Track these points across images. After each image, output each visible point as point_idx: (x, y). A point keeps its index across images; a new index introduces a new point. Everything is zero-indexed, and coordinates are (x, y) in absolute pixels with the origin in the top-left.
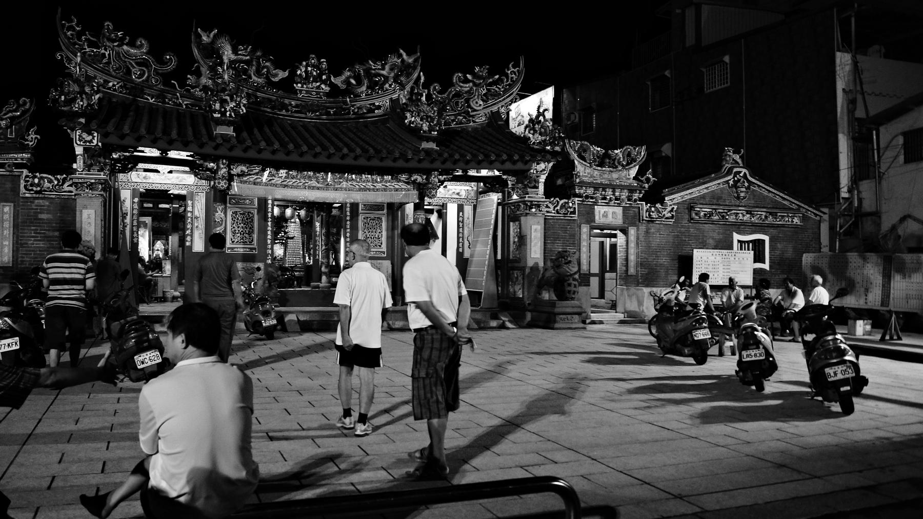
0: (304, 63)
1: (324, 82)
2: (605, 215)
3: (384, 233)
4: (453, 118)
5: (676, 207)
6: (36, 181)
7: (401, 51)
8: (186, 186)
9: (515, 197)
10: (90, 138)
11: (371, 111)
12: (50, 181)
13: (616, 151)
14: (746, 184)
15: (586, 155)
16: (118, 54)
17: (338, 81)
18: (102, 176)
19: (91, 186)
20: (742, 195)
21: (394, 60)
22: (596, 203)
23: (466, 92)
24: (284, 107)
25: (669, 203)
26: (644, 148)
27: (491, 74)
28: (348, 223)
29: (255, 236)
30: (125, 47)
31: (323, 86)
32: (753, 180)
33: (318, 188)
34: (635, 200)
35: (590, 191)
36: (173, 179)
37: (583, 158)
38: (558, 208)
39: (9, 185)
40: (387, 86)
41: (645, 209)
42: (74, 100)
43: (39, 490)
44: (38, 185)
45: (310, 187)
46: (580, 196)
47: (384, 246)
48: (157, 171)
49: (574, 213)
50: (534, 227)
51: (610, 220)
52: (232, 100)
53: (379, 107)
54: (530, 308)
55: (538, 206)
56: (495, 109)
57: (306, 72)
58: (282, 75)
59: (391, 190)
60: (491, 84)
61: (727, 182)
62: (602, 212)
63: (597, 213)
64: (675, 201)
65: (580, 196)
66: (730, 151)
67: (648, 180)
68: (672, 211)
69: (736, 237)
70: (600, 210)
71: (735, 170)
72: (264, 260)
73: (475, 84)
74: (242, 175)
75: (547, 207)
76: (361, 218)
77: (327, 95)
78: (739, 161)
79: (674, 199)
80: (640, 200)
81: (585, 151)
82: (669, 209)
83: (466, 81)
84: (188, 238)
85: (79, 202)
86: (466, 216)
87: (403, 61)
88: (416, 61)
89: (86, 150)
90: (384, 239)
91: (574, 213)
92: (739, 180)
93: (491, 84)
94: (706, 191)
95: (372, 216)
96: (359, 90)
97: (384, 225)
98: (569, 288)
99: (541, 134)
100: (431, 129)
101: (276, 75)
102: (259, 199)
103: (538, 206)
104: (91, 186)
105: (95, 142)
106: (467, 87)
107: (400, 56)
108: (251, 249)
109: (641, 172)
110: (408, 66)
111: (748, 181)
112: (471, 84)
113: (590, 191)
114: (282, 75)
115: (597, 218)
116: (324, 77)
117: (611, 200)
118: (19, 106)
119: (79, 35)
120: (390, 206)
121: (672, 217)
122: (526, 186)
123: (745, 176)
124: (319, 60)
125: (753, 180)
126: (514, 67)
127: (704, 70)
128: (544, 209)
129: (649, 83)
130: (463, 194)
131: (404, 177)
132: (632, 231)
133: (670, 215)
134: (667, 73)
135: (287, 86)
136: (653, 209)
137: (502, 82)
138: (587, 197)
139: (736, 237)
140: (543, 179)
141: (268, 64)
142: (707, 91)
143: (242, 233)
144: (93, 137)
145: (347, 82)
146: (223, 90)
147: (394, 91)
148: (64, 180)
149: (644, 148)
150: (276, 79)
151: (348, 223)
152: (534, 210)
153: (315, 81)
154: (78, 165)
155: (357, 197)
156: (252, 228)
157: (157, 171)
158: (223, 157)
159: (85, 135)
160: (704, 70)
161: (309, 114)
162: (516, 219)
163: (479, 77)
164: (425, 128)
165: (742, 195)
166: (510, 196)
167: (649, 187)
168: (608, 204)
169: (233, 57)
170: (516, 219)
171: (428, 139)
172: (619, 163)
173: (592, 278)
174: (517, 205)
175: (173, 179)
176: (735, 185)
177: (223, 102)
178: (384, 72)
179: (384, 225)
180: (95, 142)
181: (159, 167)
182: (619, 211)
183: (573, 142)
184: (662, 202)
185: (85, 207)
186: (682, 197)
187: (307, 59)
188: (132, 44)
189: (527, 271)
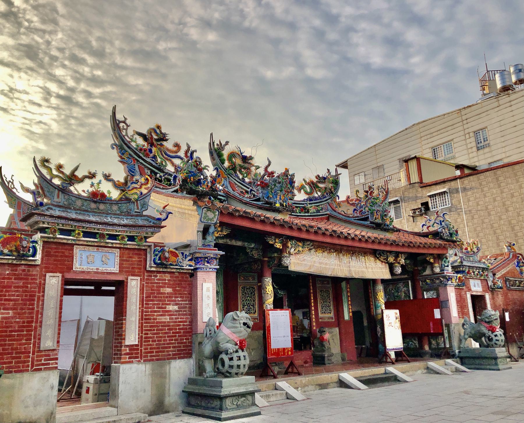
28: (312, 295)
144: (215, 215)
151: (312, 295)
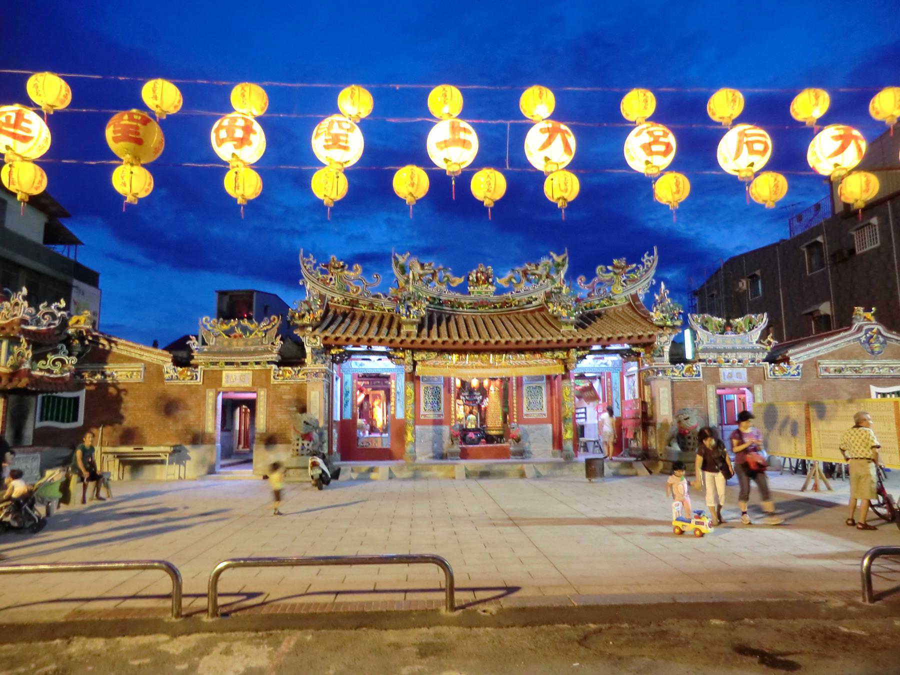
0: (475, 271)
1: (491, 284)
2: (730, 376)
3: (545, 399)
4: (597, 302)
5: (801, 365)
6: (281, 373)
7: (552, 253)
8: (390, 369)
9: (646, 365)
10: (315, 341)
11: (529, 302)
12: (290, 372)
13: (737, 320)
14: (881, 339)
15: (709, 326)
16: (341, 277)
17: (502, 282)
18: (324, 367)
19: (316, 375)
20: (877, 350)
21: (544, 260)
22: (720, 366)
23: (608, 281)
24: (461, 305)
25: (794, 362)
26: (765, 314)
27: (629, 262)
29: (442, 405)
30: (346, 272)
31: (490, 287)
32: (889, 335)
33: (483, 367)
34: (758, 362)
35: (712, 356)
36: (378, 364)
37: (706, 329)
38: (684, 372)
39: (264, 376)
40: (541, 282)
41: (769, 368)
42: (303, 316)
43: (174, 480)
44: (282, 375)
45: (476, 367)
46: (703, 361)
47: (545, 411)
48: (369, 360)
49: (699, 375)
50: (661, 389)
51: (736, 380)
52: (415, 305)
53: (536, 299)
54: (664, 458)
55: (664, 371)
56: (633, 292)
57: (477, 278)
58: (459, 281)
59: (541, 365)
60: (630, 272)
61: (859, 339)
62: (726, 374)
63: (721, 374)
64: (800, 360)
65: (703, 361)
66: (859, 310)
67: (770, 343)
68: (798, 368)
69: (874, 389)
70: (725, 371)
71: (866, 327)
72: (449, 423)
73: (615, 274)
74: (423, 360)
75: (673, 371)
76: (525, 387)
77: (496, 293)
78: (872, 318)
79: (799, 356)
80: (764, 361)
81: (707, 322)
82: (795, 367)
83: (608, 271)
84: (393, 408)
85: (309, 386)
86: (614, 381)
87: (553, 261)
88: (564, 260)
89: (313, 349)
90: (544, 404)
91: (699, 375)
92: (872, 337)
93: (630, 272)
94: (834, 349)
95: (534, 385)
96: (519, 287)
97: (544, 392)
98: (689, 441)
99: (662, 312)
100: (569, 315)
101: (453, 282)
102: (444, 378)
103: (664, 371)
104: (316, 375)
105: (318, 343)
106: (608, 276)
107: (551, 257)
108: (439, 415)
109: (764, 336)
110: (559, 265)
111: (883, 336)
112: (612, 274)
113: (712, 356)
114: (459, 281)
115: (722, 378)
116: (491, 280)
117: (733, 362)
118: (271, 322)
119: (315, 266)
120: (549, 377)
121: (799, 374)
122: (653, 356)
123: (879, 332)
124: (486, 267)
125: (889, 335)
126: (649, 255)
127: (854, 233)
128: (669, 373)
129: (805, 249)
130: (610, 364)
131: (549, 354)
132: (758, 389)
133: (795, 373)
134: (820, 239)
135: (462, 289)
136: (777, 368)
137: (638, 268)
138: (710, 361)
139: (874, 389)
140: (667, 349)
141: (448, 274)
142: (858, 252)
143: (432, 404)
145: (510, 281)
146: (409, 299)
147: (548, 286)
148: (299, 371)
149: (765, 314)
150: (454, 285)
152: (661, 375)
153: (484, 283)
154: (308, 360)
155: (524, 372)
156: (439, 399)
157: (369, 360)
158: (407, 349)
159: (312, 339)
160: (854, 233)
161: (480, 310)
162: (647, 383)
163: (617, 268)
164: (564, 313)
165: (877, 350)
166: (643, 365)
167: (772, 349)
168: (731, 367)
169: (421, 272)
170: (647, 383)
171: (566, 324)
172: (741, 330)
173: (31, 443)
174: (647, 371)
175: (378, 364)
176: (868, 341)
177: (408, 308)
178: (537, 272)
179: (544, 392)
180: (318, 343)
181: (371, 357)
182: (744, 371)
183: (696, 316)
184: (786, 360)
185: (313, 390)
186: (809, 355)
187: (476, 267)
188: (350, 269)
189: (658, 426)
